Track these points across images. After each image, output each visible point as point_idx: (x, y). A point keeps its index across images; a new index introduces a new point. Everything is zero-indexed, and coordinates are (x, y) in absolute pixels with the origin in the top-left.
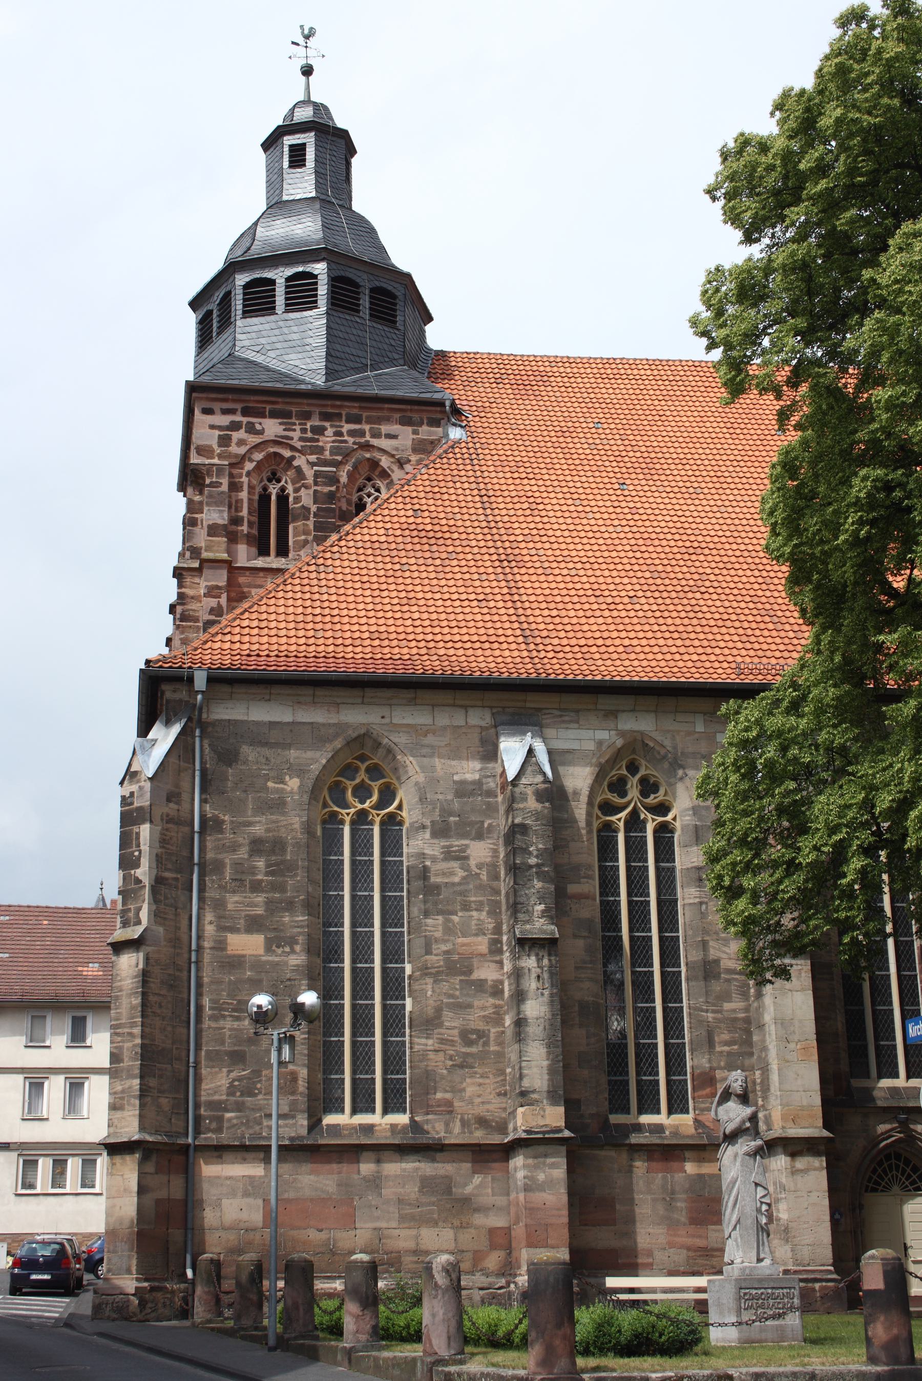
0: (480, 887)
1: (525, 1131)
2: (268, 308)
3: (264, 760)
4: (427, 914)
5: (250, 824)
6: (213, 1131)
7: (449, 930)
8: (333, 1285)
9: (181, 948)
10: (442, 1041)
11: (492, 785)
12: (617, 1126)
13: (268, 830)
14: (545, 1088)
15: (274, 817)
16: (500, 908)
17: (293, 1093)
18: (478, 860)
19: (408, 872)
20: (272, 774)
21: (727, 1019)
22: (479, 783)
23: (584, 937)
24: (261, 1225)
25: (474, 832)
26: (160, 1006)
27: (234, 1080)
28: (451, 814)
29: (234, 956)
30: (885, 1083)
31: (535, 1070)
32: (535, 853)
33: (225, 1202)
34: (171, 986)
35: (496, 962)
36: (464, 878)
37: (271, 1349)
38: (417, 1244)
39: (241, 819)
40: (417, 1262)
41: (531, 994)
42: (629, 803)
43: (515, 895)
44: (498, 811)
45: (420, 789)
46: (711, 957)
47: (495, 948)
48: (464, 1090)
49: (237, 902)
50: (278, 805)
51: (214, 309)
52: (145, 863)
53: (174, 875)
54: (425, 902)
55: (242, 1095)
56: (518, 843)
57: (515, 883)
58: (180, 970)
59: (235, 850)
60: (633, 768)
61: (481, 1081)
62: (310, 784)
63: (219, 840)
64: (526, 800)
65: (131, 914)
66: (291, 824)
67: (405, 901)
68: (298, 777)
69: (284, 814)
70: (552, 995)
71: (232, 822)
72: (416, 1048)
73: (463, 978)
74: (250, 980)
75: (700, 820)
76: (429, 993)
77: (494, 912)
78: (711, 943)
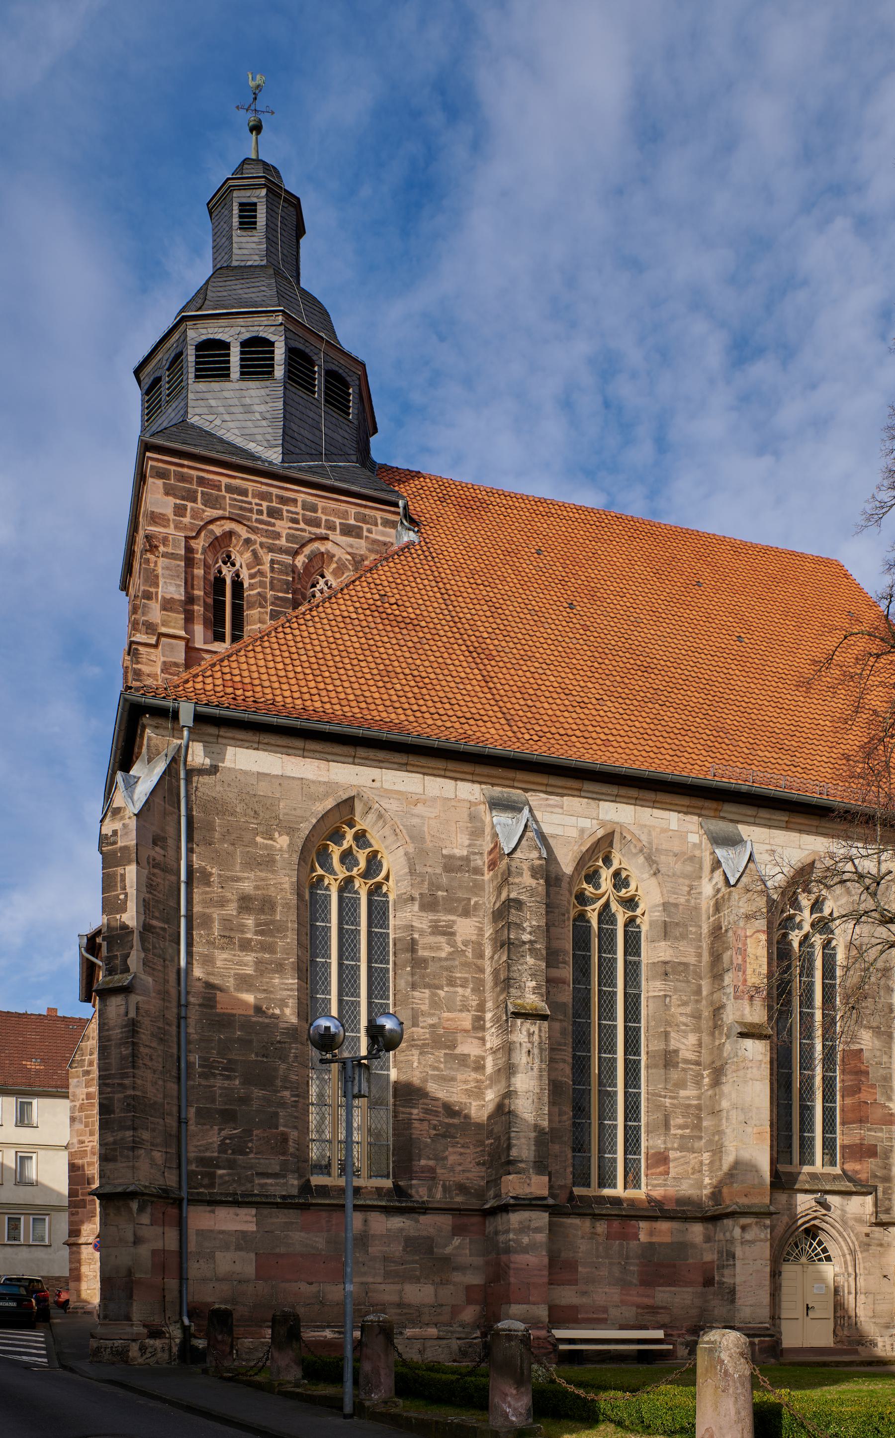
0: (465, 965)
1: (512, 1197)
2: (223, 374)
3: (252, 813)
4: (414, 986)
5: (238, 879)
6: (205, 1187)
7: (435, 1004)
8: (324, 1334)
9: (170, 1002)
10: (427, 1111)
11: (479, 862)
12: (581, 1197)
13: (257, 888)
14: (532, 1159)
15: (263, 875)
16: (484, 986)
17: (284, 1154)
18: (464, 937)
19: (395, 944)
20: (261, 829)
21: (682, 1105)
22: (467, 859)
23: (561, 1021)
24: (253, 1277)
25: (460, 909)
26: (151, 1059)
27: (225, 1138)
28: (439, 888)
29: (224, 1014)
30: (806, 1169)
31: (523, 1140)
32: (529, 929)
33: (218, 1255)
34: (161, 1039)
35: (479, 1038)
36: (450, 954)
37: (346, 1417)
38: (401, 1298)
39: (229, 874)
40: (400, 1314)
41: (521, 1068)
42: (603, 895)
43: (509, 971)
44: (484, 890)
45: (409, 859)
46: (672, 1047)
47: (479, 1025)
48: (446, 1158)
49: (225, 960)
50: (268, 862)
51: (159, 377)
52: (132, 906)
53: (162, 925)
54: (413, 974)
55: (233, 1153)
56: (512, 918)
57: (509, 958)
58: (170, 1025)
59: (223, 906)
60: (607, 861)
61: (462, 1150)
62: (300, 843)
63: (207, 893)
64: (521, 874)
65: (118, 962)
66: (281, 884)
67: (391, 973)
68: (288, 834)
69: (273, 872)
70: (541, 1070)
71: (220, 876)
72: (401, 1117)
73: (447, 1051)
74: (240, 1040)
75: (669, 916)
76: (415, 1064)
77: (479, 988)
78: (672, 1034)
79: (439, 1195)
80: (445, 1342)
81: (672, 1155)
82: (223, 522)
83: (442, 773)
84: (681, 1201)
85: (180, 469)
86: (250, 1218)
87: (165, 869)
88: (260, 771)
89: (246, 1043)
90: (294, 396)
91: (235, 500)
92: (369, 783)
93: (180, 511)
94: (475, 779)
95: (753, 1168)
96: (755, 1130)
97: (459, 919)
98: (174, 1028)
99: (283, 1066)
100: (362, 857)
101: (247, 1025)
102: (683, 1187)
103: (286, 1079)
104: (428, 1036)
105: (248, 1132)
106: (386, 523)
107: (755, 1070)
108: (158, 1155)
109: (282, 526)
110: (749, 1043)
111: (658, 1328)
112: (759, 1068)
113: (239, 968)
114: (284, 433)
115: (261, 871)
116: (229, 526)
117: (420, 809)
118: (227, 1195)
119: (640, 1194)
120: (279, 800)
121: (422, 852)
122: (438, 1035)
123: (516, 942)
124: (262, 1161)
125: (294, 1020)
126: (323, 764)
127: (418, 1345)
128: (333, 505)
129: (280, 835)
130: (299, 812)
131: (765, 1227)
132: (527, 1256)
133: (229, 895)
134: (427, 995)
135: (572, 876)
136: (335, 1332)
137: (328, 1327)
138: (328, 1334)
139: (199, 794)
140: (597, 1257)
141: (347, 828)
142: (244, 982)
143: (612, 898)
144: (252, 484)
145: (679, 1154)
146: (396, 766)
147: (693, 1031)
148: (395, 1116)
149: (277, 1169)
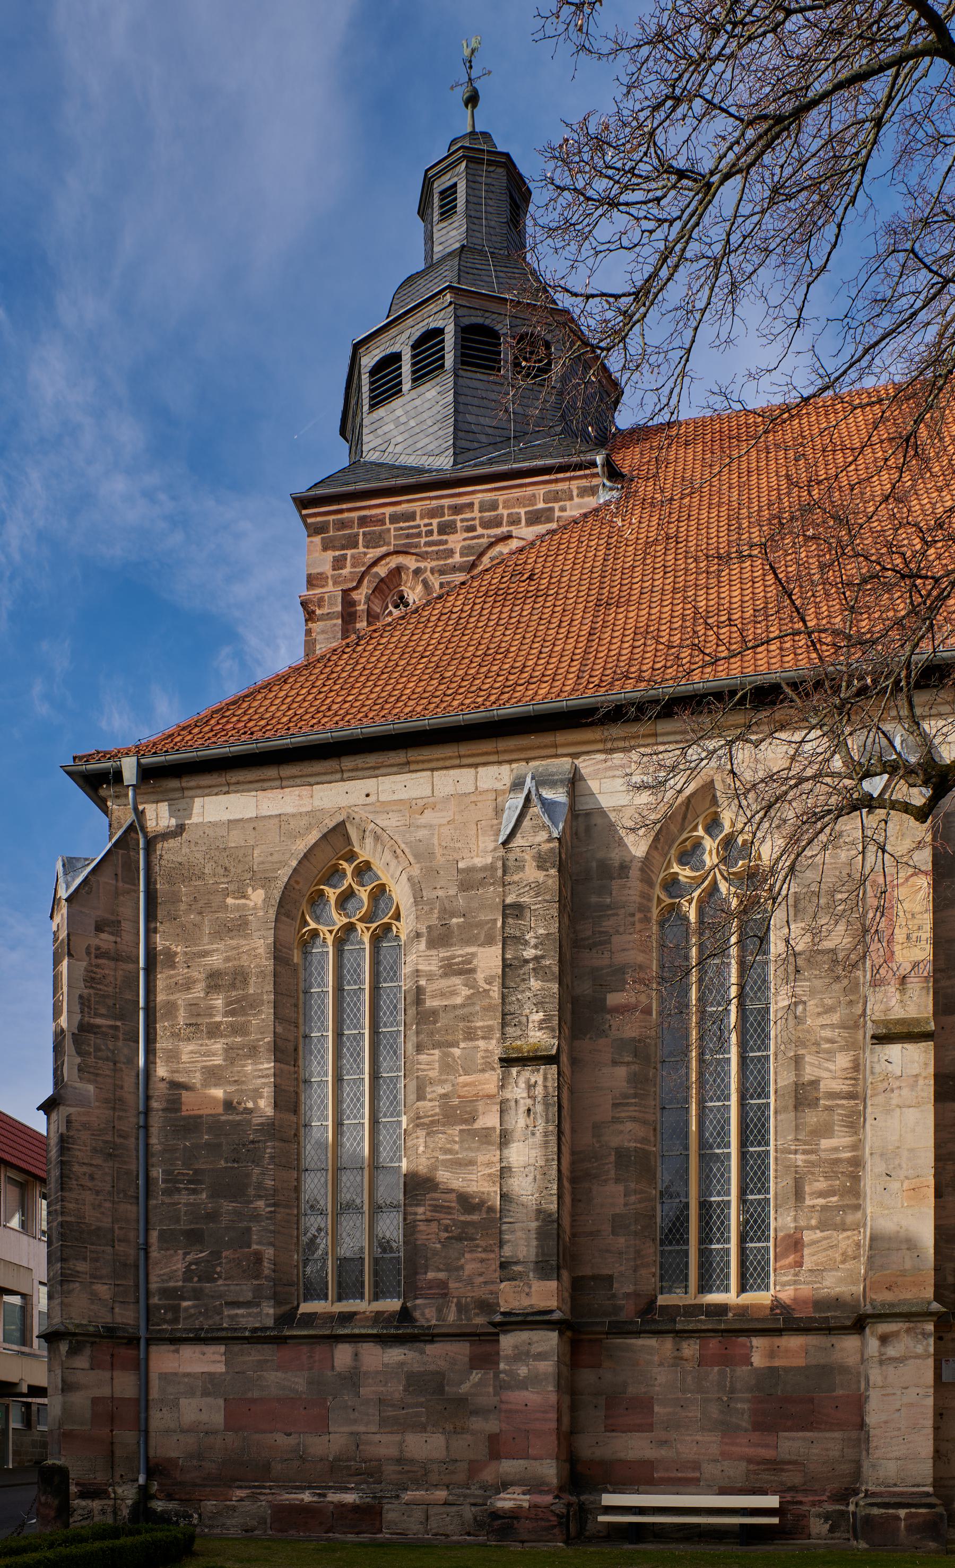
3: (222, 871)
4: (419, 1048)
5: (205, 954)
7: (447, 1067)
8: (301, 1496)
10: (436, 1208)
14: (533, 1258)
15: (233, 942)
20: (232, 887)
23: (628, 1064)
24: (222, 1427)
27: (191, 1264)
28: (453, 915)
29: (190, 1117)
31: (519, 1234)
32: (533, 942)
33: (183, 1402)
34: (110, 1155)
36: (469, 997)
38: (401, 1451)
39: (196, 949)
40: (400, 1473)
41: (518, 1134)
46: (807, 1078)
48: (462, 1268)
49: (192, 1052)
50: (239, 926)
55: (199, 1281)
59: (189, 988)
61: (483, 1255)
62: (277, 894)
63: (171, 977)
66: (255, 949)
68: (263, 887)
69: (245, 936)
70: (546, 1134)
71: (186, 953)
73: (464, 1127)
74: (208, 1145)
76: (421, 1149)
78: (808, 1059)
79: (452, 1317)
80: (454, 1509)
81: (808, 1236)
82: (388, 560)
83: (457, 762)
84: (820, 1304)
85: (339, 516)
86: (218, 1357)
87: (117, 957)
88: (231, 818)
89: (213, 1148)
90: (468, 382)
91: (402, 529)
92: (363, 800)
93: (339, 563)
94: (501, 758)
95: (911, 1244)
96: (906, 1185)
97: (481, 949)
98: (133, 1140)
99: (257, 1171)
100: (363, 894)
101: (216, 1126)
102: (826, 1283)
103: (260, 1186)
104: (437, 1110)
105: (216, 1254)
106: (583, 492)
107: (905, 1092)
108: (103, 1290)
109: (456, 541)
110: (894, 1051)
111: (774, 1493)
112: (913, 1087)
113: (206, 1061)
114: (456, 429)
115: (231, 938)
116: (394, 561)
117: (429, 817)
118: (190, 1330)
119: (760, 1298)
120: (253, 847)
121: (432, 872)
122: (452, 1107)
123: (516, 963)
124: (232, 1288)
125: (270, 1111)
126: (305, 791)
127: (418, 1514)
128: (517, 493)
129: (254, 890)
130: (275, 858)
131: (925, 1335)
132: (525, 1393)
133: (195, 974)
134: (436, 1057)
135: (646, 858)
136: (315, 1494)
137: (309, 1488)
138: (307, 1497)
139: (163, 863)
140: (684, 1391)
141: (345, 865)
142: (213, 1075)
143: (719, 877)
144: (417, 505)
145: (819, 1234)
146: (395, 769)
147: (842, 1049)
148: (405, 1219)
149: (249, 1296)
